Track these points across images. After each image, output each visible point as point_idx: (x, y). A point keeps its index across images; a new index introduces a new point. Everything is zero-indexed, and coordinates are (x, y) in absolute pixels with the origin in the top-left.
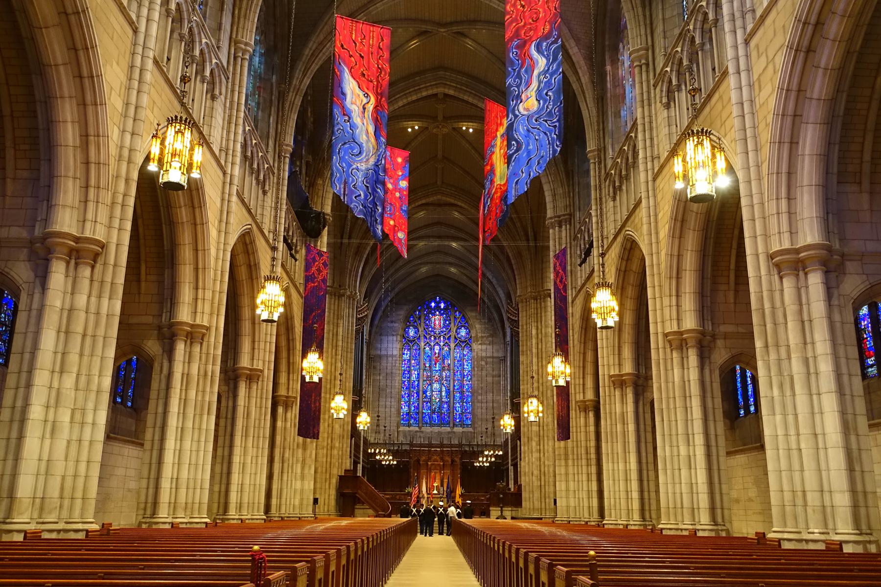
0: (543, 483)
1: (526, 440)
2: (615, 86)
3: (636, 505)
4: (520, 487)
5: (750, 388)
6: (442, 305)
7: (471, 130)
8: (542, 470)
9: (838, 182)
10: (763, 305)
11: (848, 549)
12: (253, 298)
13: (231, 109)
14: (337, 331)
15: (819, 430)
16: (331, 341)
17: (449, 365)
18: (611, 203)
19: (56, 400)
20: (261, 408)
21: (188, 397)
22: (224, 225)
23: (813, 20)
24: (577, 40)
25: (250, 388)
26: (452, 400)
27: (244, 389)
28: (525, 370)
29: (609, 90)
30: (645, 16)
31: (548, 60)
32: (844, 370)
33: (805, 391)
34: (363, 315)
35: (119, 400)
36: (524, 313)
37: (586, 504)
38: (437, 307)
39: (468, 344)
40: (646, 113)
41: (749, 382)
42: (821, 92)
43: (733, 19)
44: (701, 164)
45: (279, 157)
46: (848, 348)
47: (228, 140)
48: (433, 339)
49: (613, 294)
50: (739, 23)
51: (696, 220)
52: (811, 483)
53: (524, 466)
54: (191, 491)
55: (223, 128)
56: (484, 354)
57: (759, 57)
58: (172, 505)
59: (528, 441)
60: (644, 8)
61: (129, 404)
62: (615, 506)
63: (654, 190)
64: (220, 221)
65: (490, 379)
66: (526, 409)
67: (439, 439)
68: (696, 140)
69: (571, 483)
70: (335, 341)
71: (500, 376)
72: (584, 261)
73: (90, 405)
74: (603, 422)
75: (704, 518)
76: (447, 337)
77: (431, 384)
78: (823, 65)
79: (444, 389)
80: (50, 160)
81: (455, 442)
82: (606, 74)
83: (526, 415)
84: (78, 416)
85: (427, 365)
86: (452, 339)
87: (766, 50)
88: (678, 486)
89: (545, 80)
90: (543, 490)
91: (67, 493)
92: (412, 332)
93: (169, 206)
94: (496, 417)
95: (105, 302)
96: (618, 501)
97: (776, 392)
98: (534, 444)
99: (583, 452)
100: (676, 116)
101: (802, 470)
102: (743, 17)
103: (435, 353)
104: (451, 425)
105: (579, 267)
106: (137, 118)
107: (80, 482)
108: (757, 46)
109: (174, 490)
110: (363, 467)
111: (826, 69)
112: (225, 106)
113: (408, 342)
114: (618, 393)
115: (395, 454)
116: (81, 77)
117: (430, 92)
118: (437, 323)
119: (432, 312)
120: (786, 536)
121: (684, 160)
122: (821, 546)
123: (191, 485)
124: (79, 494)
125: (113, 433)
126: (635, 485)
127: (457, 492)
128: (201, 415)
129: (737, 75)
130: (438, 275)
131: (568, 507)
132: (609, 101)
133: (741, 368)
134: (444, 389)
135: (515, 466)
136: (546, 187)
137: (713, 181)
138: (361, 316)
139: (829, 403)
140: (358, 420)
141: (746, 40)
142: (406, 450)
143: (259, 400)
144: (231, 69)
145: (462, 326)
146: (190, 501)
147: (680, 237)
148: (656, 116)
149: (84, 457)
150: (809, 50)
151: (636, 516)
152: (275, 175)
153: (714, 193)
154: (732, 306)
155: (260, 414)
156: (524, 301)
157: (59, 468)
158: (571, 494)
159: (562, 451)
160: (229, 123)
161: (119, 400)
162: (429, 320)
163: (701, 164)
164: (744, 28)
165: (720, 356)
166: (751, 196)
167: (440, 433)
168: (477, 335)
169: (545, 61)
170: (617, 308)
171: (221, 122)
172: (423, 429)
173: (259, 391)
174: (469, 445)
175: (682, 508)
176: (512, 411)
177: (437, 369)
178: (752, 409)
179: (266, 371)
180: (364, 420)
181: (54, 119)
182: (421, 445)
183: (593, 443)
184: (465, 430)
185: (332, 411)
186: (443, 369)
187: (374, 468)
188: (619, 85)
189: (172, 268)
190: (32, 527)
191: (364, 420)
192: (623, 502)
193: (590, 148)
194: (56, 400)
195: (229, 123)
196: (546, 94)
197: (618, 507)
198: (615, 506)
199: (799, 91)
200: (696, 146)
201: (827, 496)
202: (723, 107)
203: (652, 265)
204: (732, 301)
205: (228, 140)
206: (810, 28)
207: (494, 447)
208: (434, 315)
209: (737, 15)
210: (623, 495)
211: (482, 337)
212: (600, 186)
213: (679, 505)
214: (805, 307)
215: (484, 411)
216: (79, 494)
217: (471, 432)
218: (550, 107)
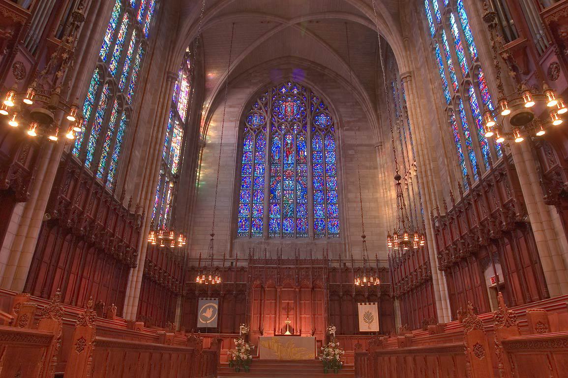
119: (280, 96)
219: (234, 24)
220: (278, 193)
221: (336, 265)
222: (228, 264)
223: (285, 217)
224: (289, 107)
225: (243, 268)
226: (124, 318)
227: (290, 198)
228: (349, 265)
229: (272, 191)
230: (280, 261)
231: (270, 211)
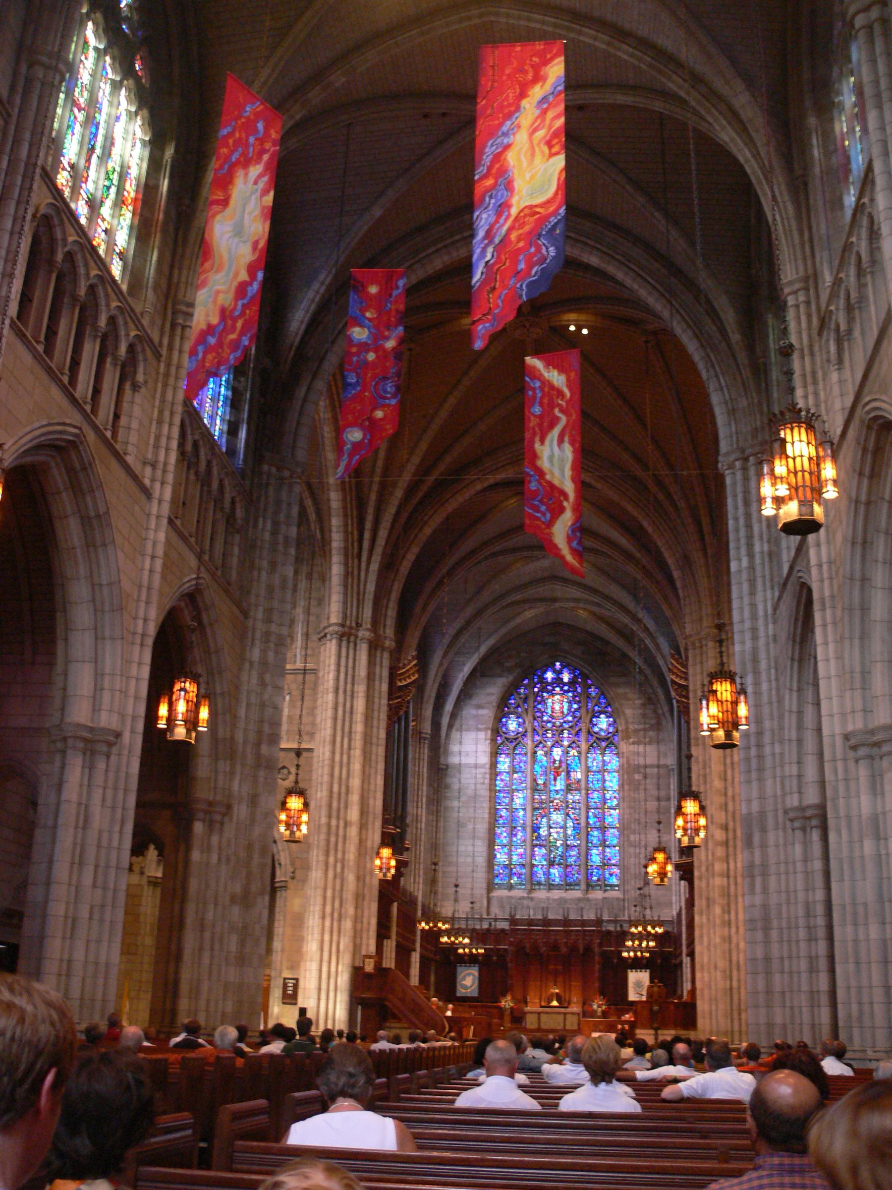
0: (735, 984)
1: (704, 902)
2: (827, 153)
6: (566, 677)
7: (585, 331)
8: (734, 958)
14: (352, 707)
16: (339, 722)
17: (579, 781)
18: (834, 376)
20: (114, 808)
25: (92, 768)
26: (584, 843)
27: (78, 770)
28: (702, 772)
29: (817, 162)
34: (409, 681)
36: (698, 666)
38: (558, 681)
39: (611, 743)
45: (174, 325)
48: (549, 735)
56: (641, 761)
59: (708, 906)
67: (561, 912)
69: (777, 978)
70: (347, 724)
71: (668, 799)
76: (574, 732)
77: (547, 816)
79: (570, 824)
81: (590, 915)
85: (540, 782)
86: (583, 735)
90: (736, 998)
92: (512, 725)
98: (718, 910)
103: (555, 761)
104: (583, 887)
110: (422, 956)
114: (863, 772)
119: (545, 686)
127: (418, 956)
130: (557, 624)
132: (818, 182)
138: (404, 683)
142: (503, 930)
143: (110, 793)
144: (18, 100)
145: (601, 713)
152: (163, 359)
155: (113, 820)
156: (698, 644)
162: (543, 702)
167: (562, 901)
168: (627, 729)
172: (535, 895)
173: (111, 775)
174: (615, 922)
177: (558, 788)
179: (127, 736)
182: (531, 922)
184: (607, 895)
186: (569, 789)
188: (836, 150)
193: (786, 277)
197: (867, 1023)
208: (552, 693)
211: (636, 731)
212: (811, 346)
217: (618, 899)
220: (543, 832)
221: (611, 928)
223: (551, 864)
229: (536, 829)
231: (533, 856)
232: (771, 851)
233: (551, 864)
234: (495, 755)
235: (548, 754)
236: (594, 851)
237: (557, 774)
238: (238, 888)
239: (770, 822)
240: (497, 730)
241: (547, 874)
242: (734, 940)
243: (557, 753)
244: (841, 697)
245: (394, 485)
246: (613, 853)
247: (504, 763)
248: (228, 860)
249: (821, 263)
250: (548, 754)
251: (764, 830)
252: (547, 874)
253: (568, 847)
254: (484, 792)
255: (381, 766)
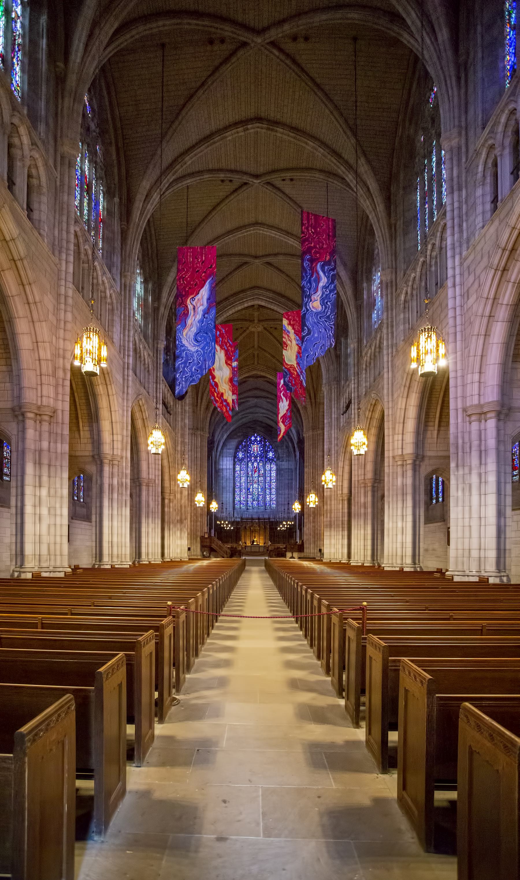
3: (369, 553)
4: (303, 541)
5: (440, 488)
9: (512, 362)
10: (457, 441)
11: (491, 581)
12: (147, 439)
13: (125, 320)
15: (483, 515)
19: (38, 504)
21: (113, 498)
22: (126, 395)
23: (510, 247)
24: (345, 265)
30: (391, 247)
31: (328, 280)
32: (503, 480)
33: (478, 493)
35: (76, 498)
37: (340, 551)
38: (256, 440)
40: (390, 316)
41: (440, 484)
42: (509, 299)
43: (453, 248)
44: (429, 351)
46: (507, 466)
47: (124, 341)
49: (364, 434)
50: (457, 250)
51: (418, 386)
52: (475, 544)
53: (305, 530)
54: (120, 548)
55: (121, 333)
57: (469, 274)
58: (110, 556)
60: (391, 241)
61: (82, 500)
62: (357, 553)
63: (392, 367)
64: (123, 392)
65: (287, 481)
66: (308, 500)
68: (427, 335)
71: (292, 479)
72: (345, 412)
73: (58, 505)
74: (353, 508)
75: (409, 560)
77: (253, 485)
78: (512, 280)
79: (260, 487)
80: (17, 359)
81: (266, 516)
82: (364, 289)
83: (308, 504)
84: (52, 511)
87: (475, 270)
88: (395, 544)
89: (326, 293)
91: (52, 552)
92: (240, 455)
93: (91, 384)
94: (290, 503)
95: (59, 445)
96: (359, 551)
97: (460, 493)
98: (311, 518)
99: (340, 523)
100: (409, 317)
101: (470, 537)
102: (461, 246)
105: (342, 416)
106: (66, 329)
107: (58, 546)
108: (469, 267)
109: (110, 548)
111: (514, 283)
112: (121, 317)
113: (235, 459)
115: (232, 523)
116: (28, 303)
117: (250, 304)
118: (255, 449)
119: (252, 442)
120: (457, 573)
121: (418, 348)
122: (476, 579)
123: (120, 545)
124: (58, 553)
125: (73, 516)
126: (369, 542)
128: (122, 507)
129: (453, 288)
131: (330, 553)
133: (436, 477)
134: (260, 487)
135: (300, 530)
136: (323, 366)
137: (436, 362)
139: (492, 500)
140: (211, 506)
141: (461, 263)
143: (154, 497)
146: (120, 553)
147: (407, 397)
148: (396, 318)
149: (58, 533)
150: (505, 269)
151: (369, 558)
153: (436, 371)
154: (435, 439)
155: (155, 505)
157: (45, 539)
158: (333, 546)
159: (328, 523)
160: (124, 329)
161: (76, 498)
162: (251, 447)
163: (429, 351)
164: (461, 254)
165: (425, 469)
166: (456, 371)
169: (326, 280)
170: (366, 443)
171: (119, 328)
175: (396, 555)
176: (299, 499)
178: (440, 499)
180: (214, 506)
181: (16, 332)
183: (346, 519)
185: (196, 503)
186: (259, 476)
187: (220, 530)
189: (97, 422)
190: (36, 569)
191: (214, 506)
192: (362, 551)
194: (38, 504)
195: (124, 329)
196: (327, 303)
198: (357, 553)
199: (495, 299)
200: (427, 339)
201: (482, 552)
202: (442, 311)
203: (389, 415)
204: (436, 437)
205: (124, 341)
206: (507, 253)
207: (288, 519)
208: (254, 444)
209: (457, 244)
210: (362, 547)
213: (395, 554)
214: (483, 442)
215: (283, 499)
216: (58, 553)
218: (329, 313)
219: (355, 39)
220: (251, 490)
221: (273, 520)
222: (233, 520)
223: (254, 500)
224: (255, 448)
225: (239, 522)
226: (195, 302)
227: (255, 493)
228: (278, 520)
229: (248, 489)
230: (252, 519)
231: (248, 498)
232: (333, 506)
233: (254, 500)
234: (234, 465)
235: (253, 464)
236: (268, 496)
237: (255, 471)
238: (179, 518)
239: (333, 498)
240: (235, 456)
241: (252, 504)
242: (316, 527)
243: (255, 464)
244: (358, 470)
245: (100, 270)
246: (274, 497)
247: (238, 468)
248: (175, 510)
249: (363, 336)
250: (253, 464)
251: (331, 500)
252: (252, 504)
253: (259, 495)
254: (232, 477)
255: (206, 475)
